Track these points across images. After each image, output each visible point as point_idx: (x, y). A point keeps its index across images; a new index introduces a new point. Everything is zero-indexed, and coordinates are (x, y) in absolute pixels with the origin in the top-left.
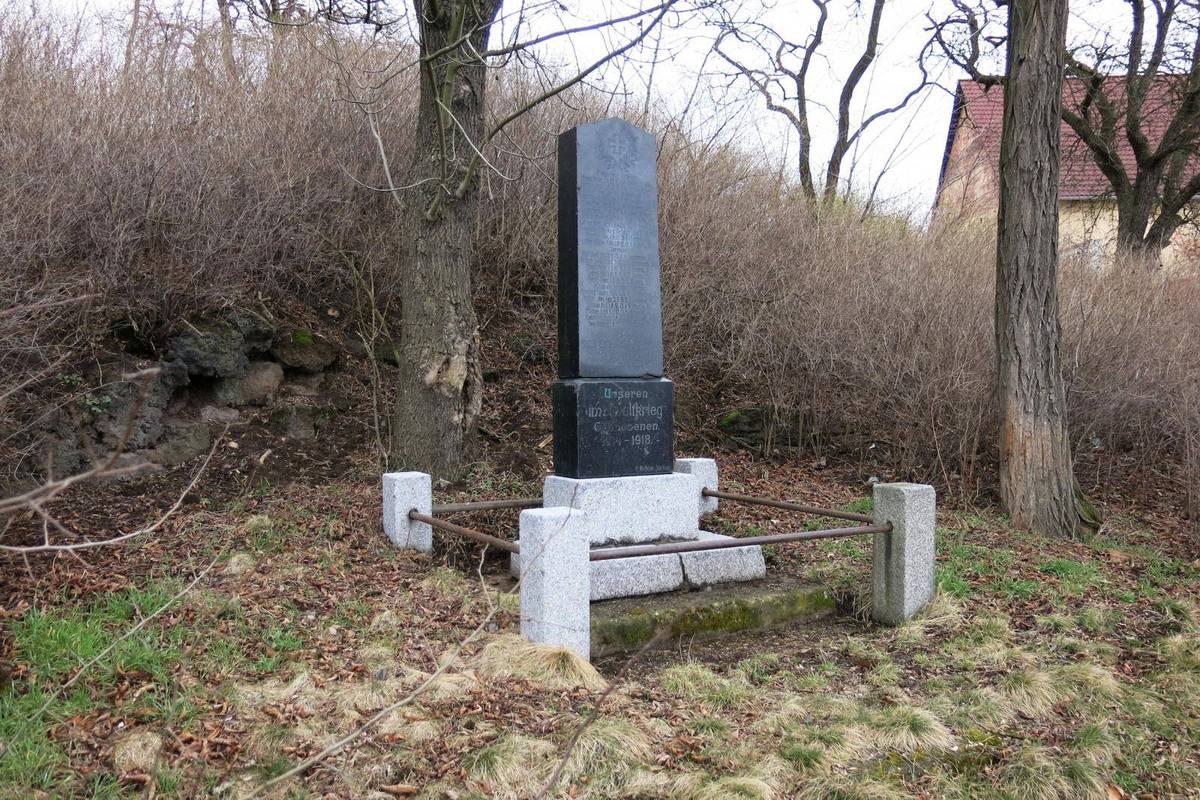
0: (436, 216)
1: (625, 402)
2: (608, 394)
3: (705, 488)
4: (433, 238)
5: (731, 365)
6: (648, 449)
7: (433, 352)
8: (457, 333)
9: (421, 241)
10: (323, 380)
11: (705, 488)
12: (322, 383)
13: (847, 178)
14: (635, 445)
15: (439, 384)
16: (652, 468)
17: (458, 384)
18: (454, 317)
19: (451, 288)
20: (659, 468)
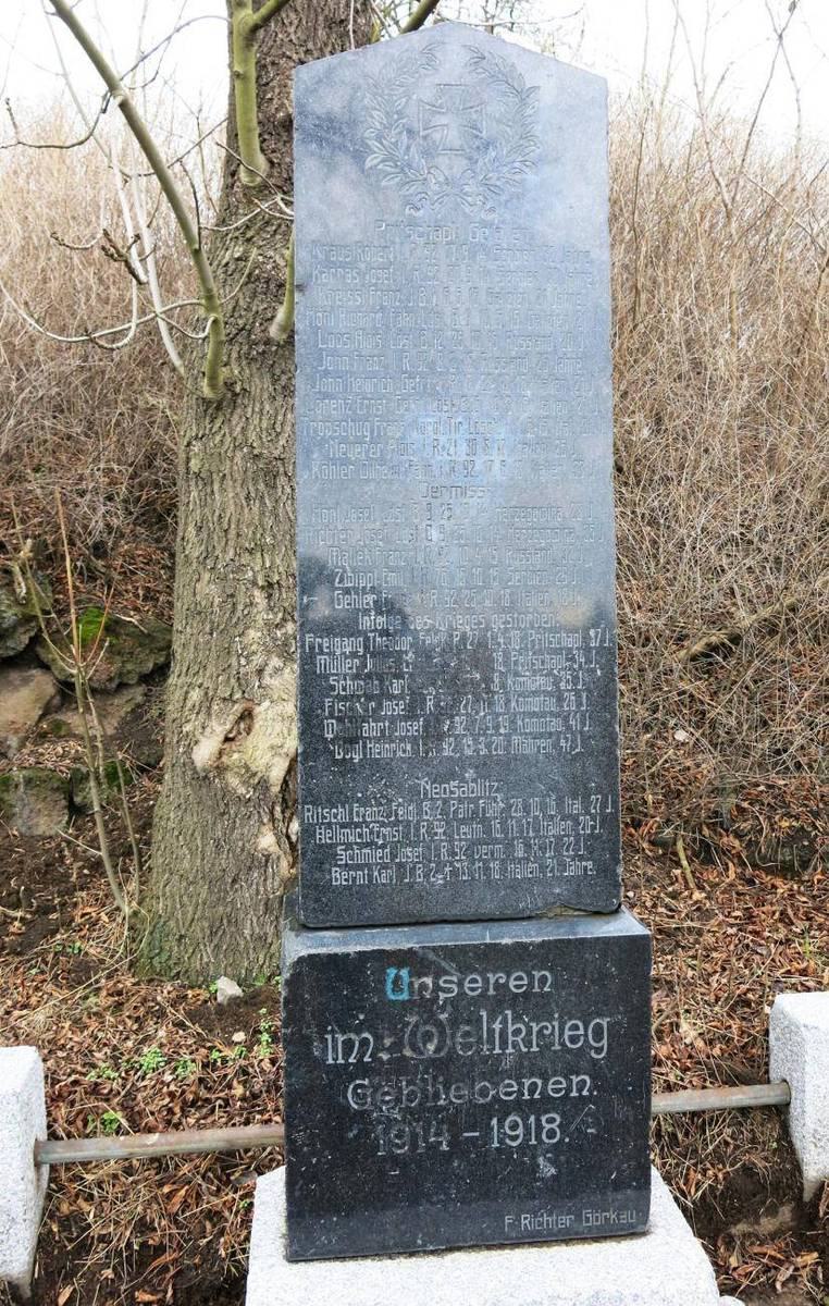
0: (223, 389)
1: (464, 1010)
2: (398, 986)
4: (218, 438)
6: (553, 1162)
7: (208, 699)
8: (269, 652)
10: (140, 699)
12: (139, 706)
13: (61, 72)
15: (221, 769)
17: (268, 767)
18: (261, 614)
19: (259, 548)
20: (593, 1219)
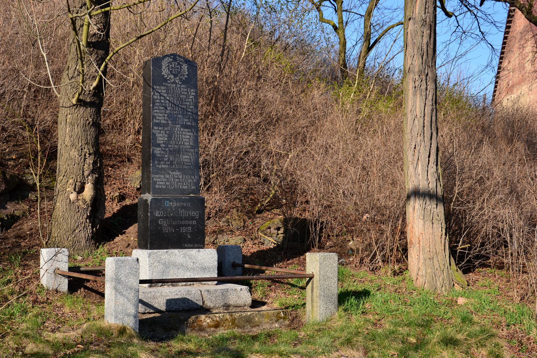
3: (234, 262)
5: (128, 76)
6: (190, 235)
9: (69, 116)
11: (234, 262)
14: (183, 233)
16: (192, 245)
20: (196, 245)
